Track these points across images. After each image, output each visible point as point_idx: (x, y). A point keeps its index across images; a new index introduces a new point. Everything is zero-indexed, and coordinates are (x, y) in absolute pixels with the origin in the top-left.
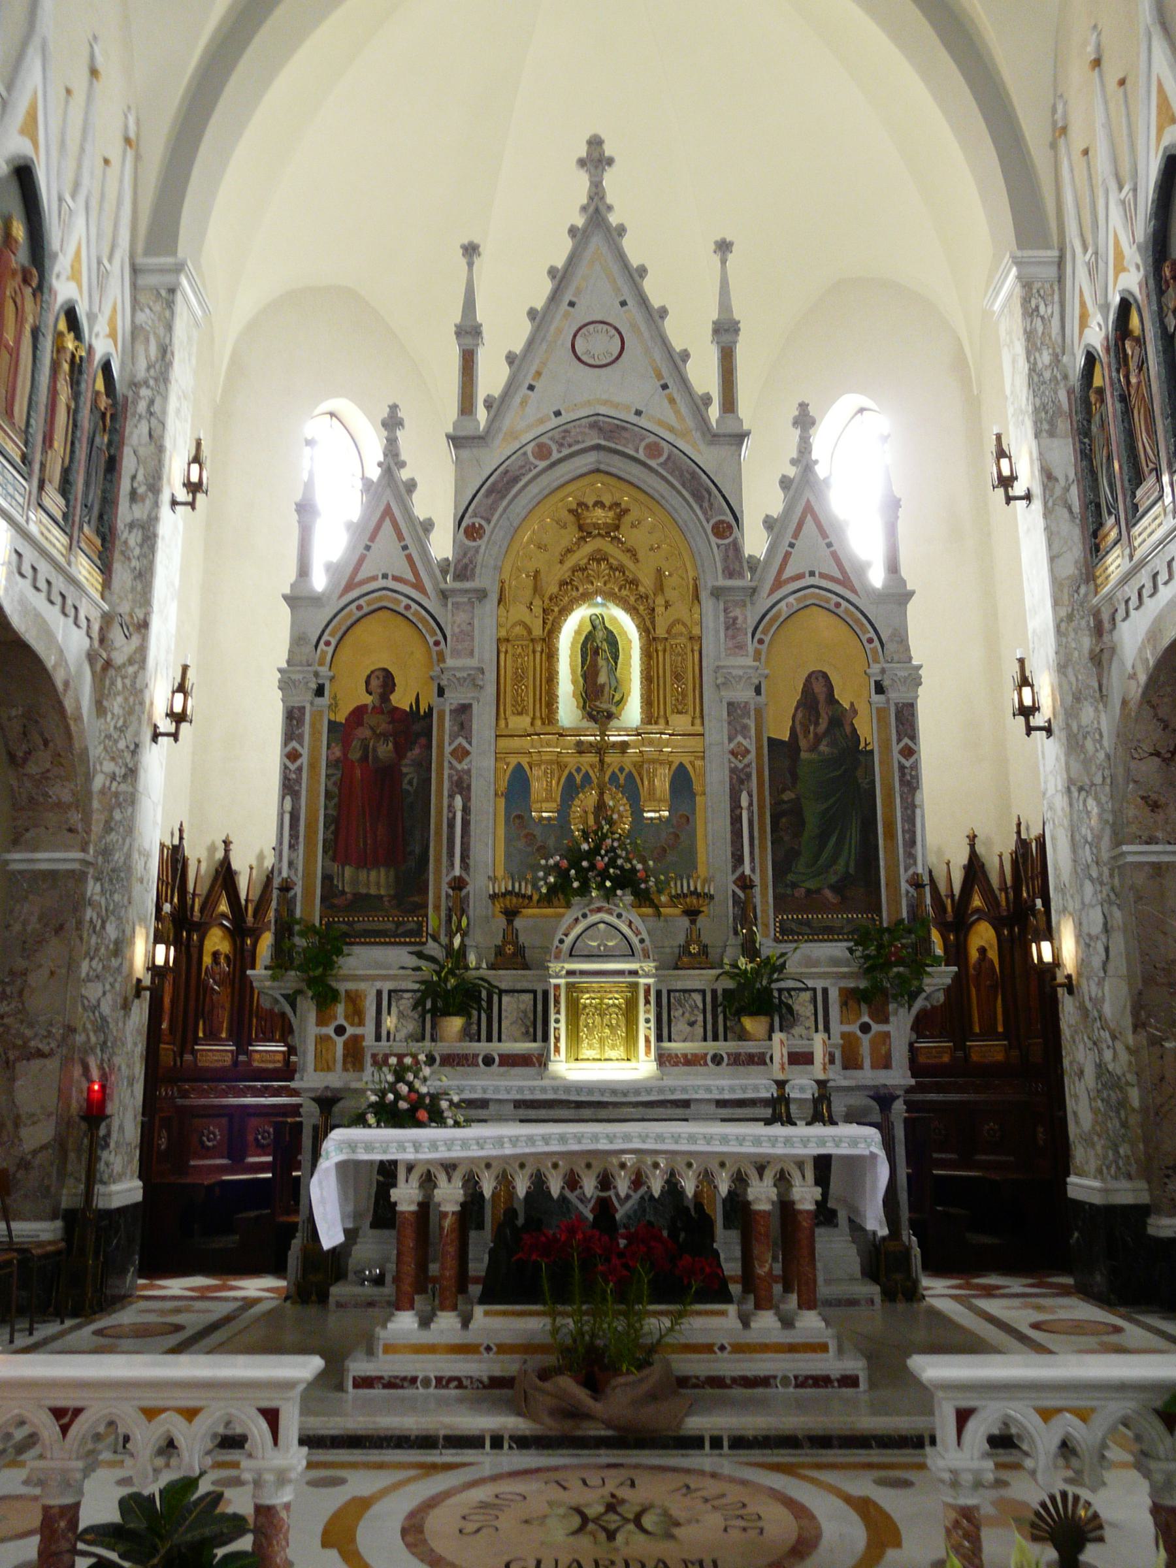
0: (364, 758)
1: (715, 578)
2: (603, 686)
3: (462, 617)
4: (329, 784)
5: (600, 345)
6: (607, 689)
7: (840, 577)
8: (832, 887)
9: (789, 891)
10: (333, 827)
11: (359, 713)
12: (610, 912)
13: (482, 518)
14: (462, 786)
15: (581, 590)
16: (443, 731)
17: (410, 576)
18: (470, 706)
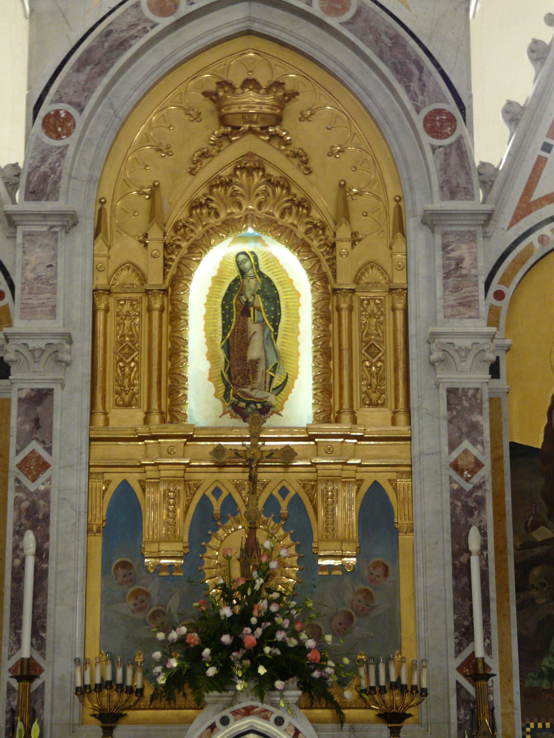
2: (256, 362)
6: (261, 368)
12: (264, 715)
13: (70, 103)
15: (223, 216)
18: (50, 391)
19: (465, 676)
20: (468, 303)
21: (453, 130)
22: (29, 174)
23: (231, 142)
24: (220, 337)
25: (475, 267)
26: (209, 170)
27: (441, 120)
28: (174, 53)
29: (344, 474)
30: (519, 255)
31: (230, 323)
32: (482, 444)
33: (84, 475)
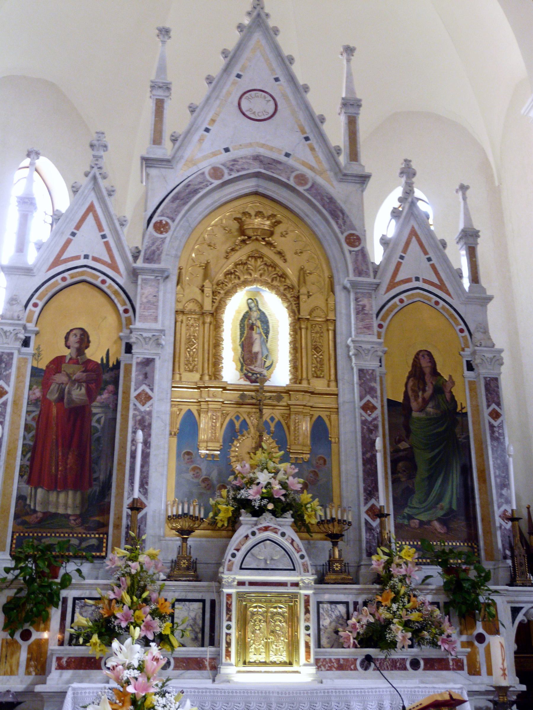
0: (61, 399)
1: (346, 278)
2: (257, 354)
3: (149, 290)
4: (29, 419)
5: (259, 105)
6: (260, 356)
7: (438, 283)
8: (439, 520)
9: (406, 522)
10: (29, 455)
11: (58, 363)
12: (275, 531)
13: (168, 217)
14: (144, 424)
15: (242, 279)
16: (130, 380)
17: (107, 259)
18: (153, 360)
19: (369, 515)
20: (368, 327)
21: (360, 244)
22: (146, 250)
23: (246, 244)
24: (239, 340)
25: (372, 310)
26: (236, 257)
27: (353, 239)
28: (220, 199)
29: (305, 411)
30: (390, 307)
31: (244, 333)
32: (376, 397)
33: (169, 405)
